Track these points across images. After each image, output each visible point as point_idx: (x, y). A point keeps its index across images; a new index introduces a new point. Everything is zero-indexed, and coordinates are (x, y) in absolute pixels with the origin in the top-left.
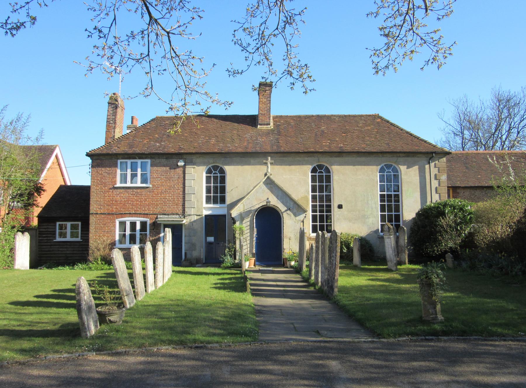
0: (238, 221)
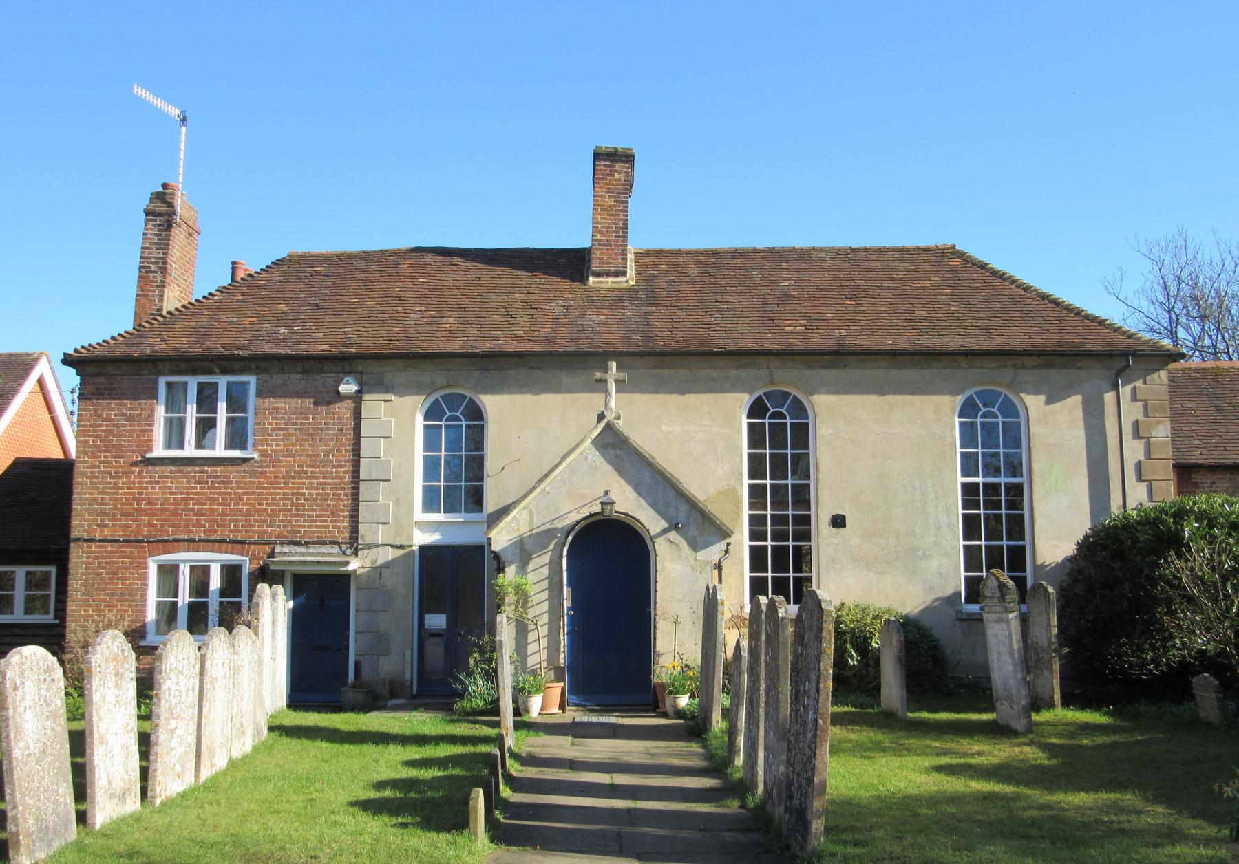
0: (511, 563)
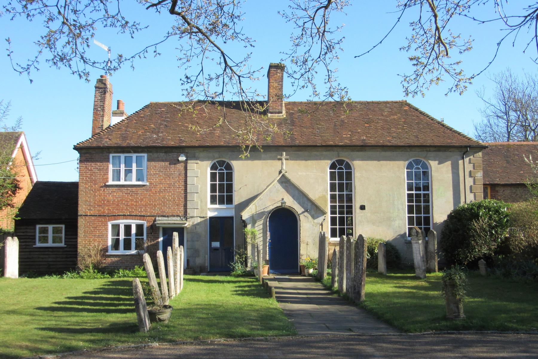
0: (249, 224)
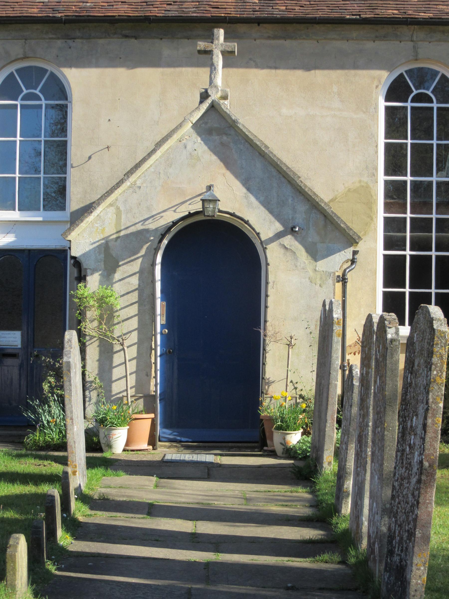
0: (94, 271)
